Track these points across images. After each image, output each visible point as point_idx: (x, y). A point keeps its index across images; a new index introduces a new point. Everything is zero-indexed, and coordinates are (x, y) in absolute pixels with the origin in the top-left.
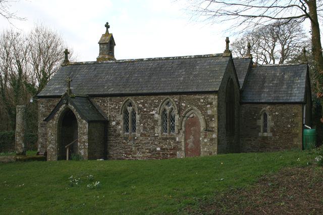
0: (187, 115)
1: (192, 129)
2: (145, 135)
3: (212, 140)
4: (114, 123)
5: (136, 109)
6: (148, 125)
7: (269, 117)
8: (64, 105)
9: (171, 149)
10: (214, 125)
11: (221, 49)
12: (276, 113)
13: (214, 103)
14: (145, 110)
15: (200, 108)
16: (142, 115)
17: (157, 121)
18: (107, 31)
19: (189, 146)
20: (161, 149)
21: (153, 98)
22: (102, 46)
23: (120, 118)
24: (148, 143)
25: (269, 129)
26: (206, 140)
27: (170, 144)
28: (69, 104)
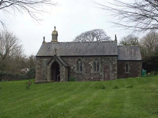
0: (105, 65)
1: (107, 70)
3: (115, 74)
4: (72, 68)
5: (83, 62)
6: (88, 68)
7: (129, 66)
8: (53, 60)
9: (98, 78)
10: (116, 68)
11: (113, 39)
12: (131, 64)
13: (116, 60)
14: (86, 62)
16: (85, 64)
17: (92, 67)
18: (55, 30)
19: (106, 77)
20: (93, 78)
21: (90, 58)
22: (53, 36)
23: (75, 66)
25: (128, 71)
26: (112, 74)
27: (97, 76)
28: (56, 60)
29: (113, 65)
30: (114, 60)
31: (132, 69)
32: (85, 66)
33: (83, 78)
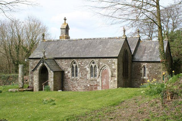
2: (82, 78)
3: (115, 81)
6: (83, 73)
7: (146, 69)
8: (42, 63)
10: (116, 73)
12: (150, 67)
14: (82, 66)
15: (109, 65)
17: (88, 71)
21: (86, 60)
22: (62, 30)
24: (84, 82)
25: (146, 75)
26: (112, 81)
27: (94, 83)
29: (113, 69)
30: (114, 63)
31: (151, 73)
32: (81, 70)
33: (79, 85)
